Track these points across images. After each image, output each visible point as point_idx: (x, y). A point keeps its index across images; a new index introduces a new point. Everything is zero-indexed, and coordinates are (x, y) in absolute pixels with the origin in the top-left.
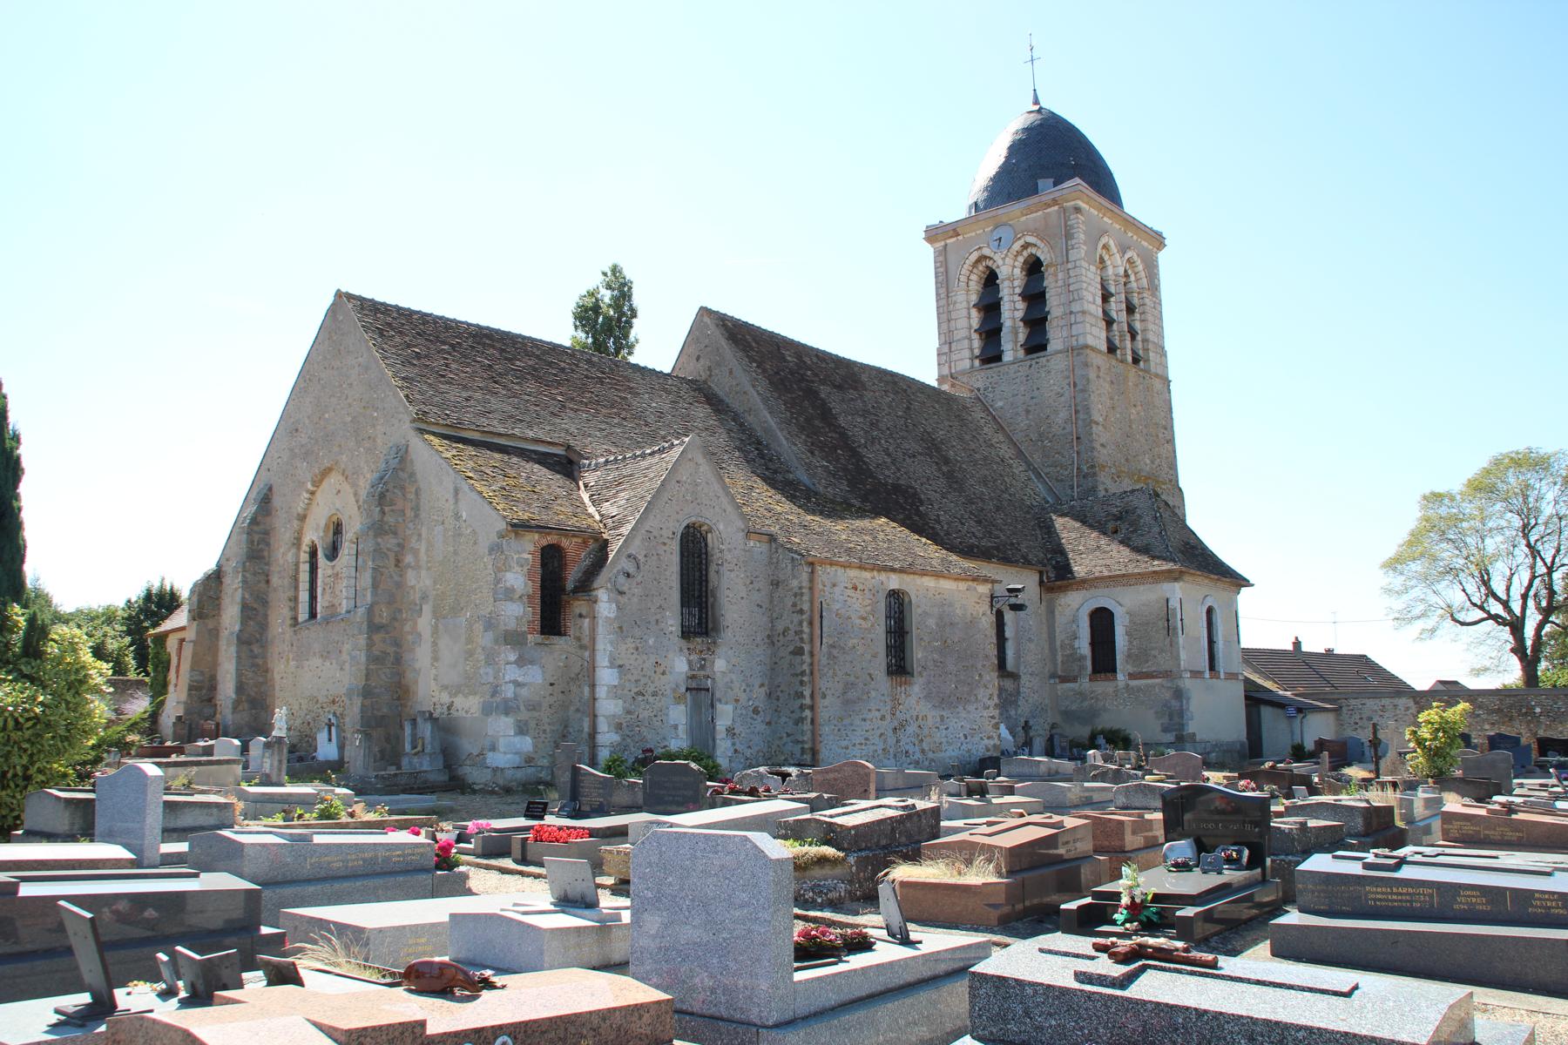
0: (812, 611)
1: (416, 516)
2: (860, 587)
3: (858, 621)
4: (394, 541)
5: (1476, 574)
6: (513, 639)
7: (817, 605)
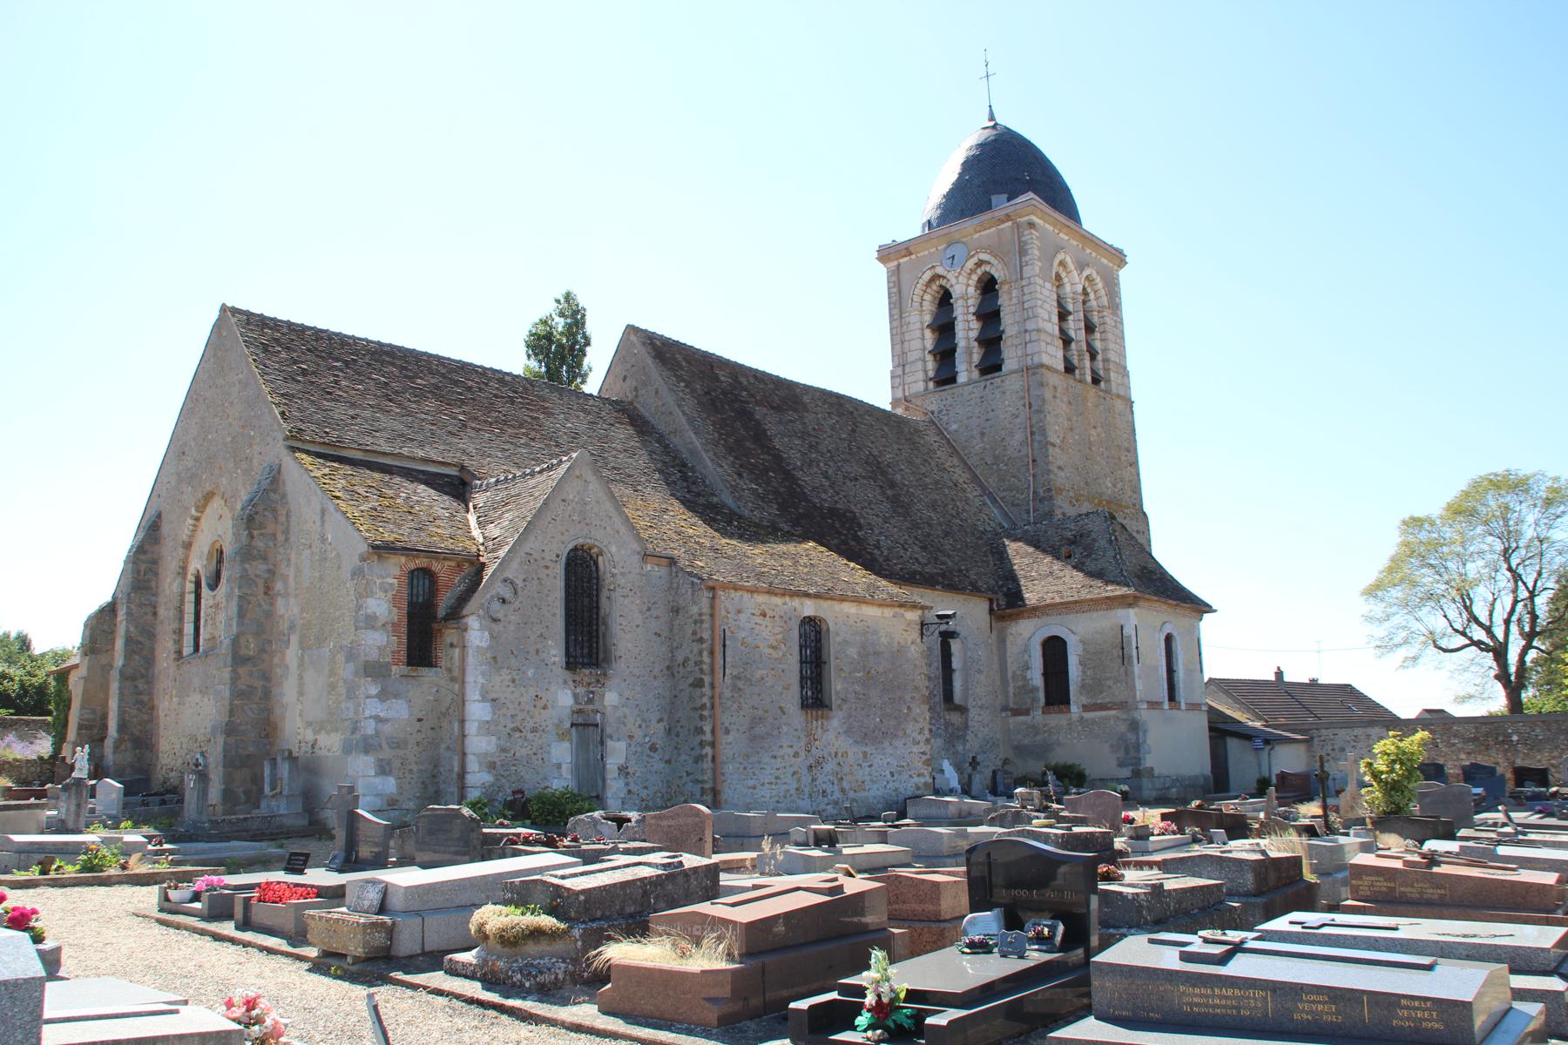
0: (713, 639)
1: (287, 540)
2: (769, 613)
3: (767, 651)
4: (265, 567)
5: (1458, 598)
6: (374, 670)
7: (718, 633)
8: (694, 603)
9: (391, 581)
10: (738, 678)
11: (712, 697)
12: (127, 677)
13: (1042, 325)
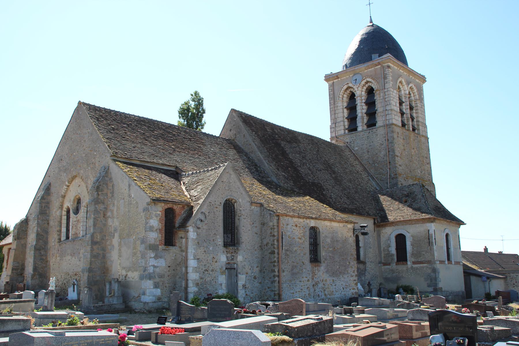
0: (278, 235)
1: (113, 196)
2: (298, 225)
3: (298, 240)
4: (103, 206)
6: (153, 247)
7: (281, 233)
8: (271, 221)
9: (159, 213)
10: (287, 250)
11: (278, 258)
12: (37, 249)
13: (393, 107)
